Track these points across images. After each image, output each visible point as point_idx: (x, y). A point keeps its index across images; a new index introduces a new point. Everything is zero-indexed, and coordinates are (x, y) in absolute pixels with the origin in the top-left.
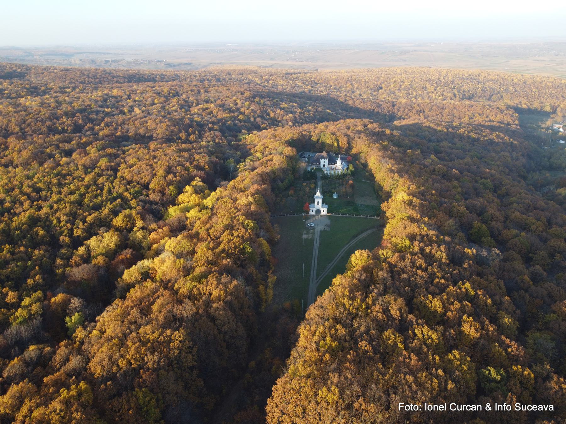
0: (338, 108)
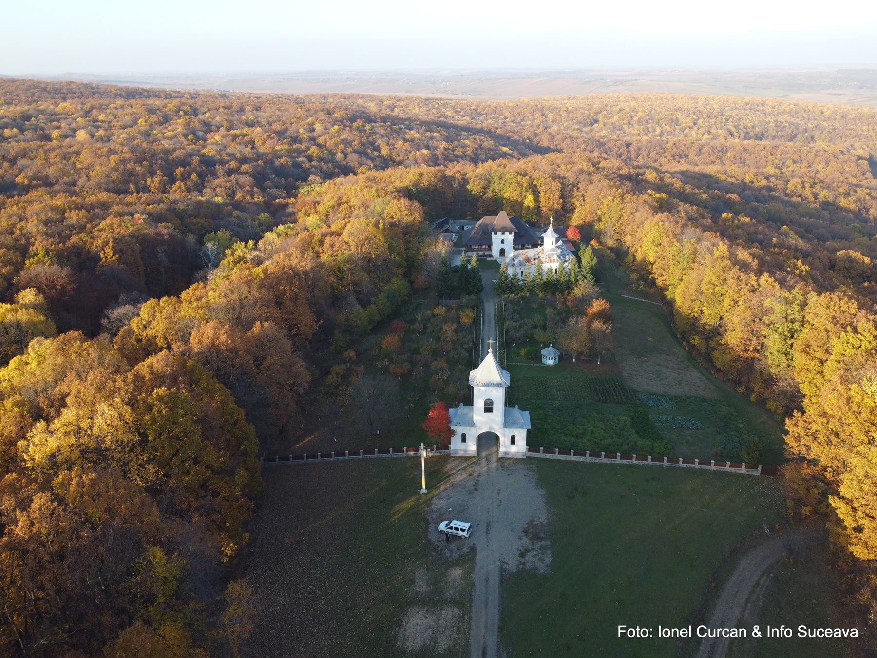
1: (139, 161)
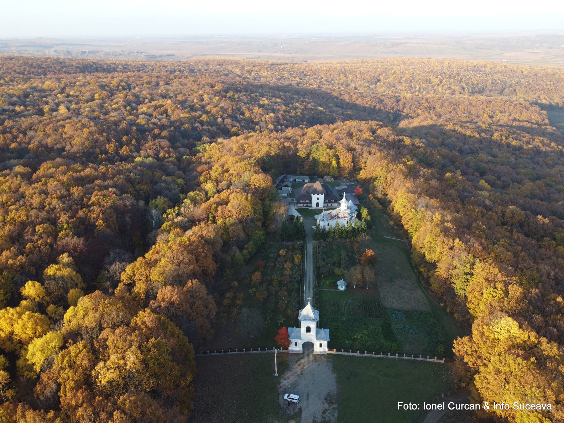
0: (332, 105)
1: (101, 132)
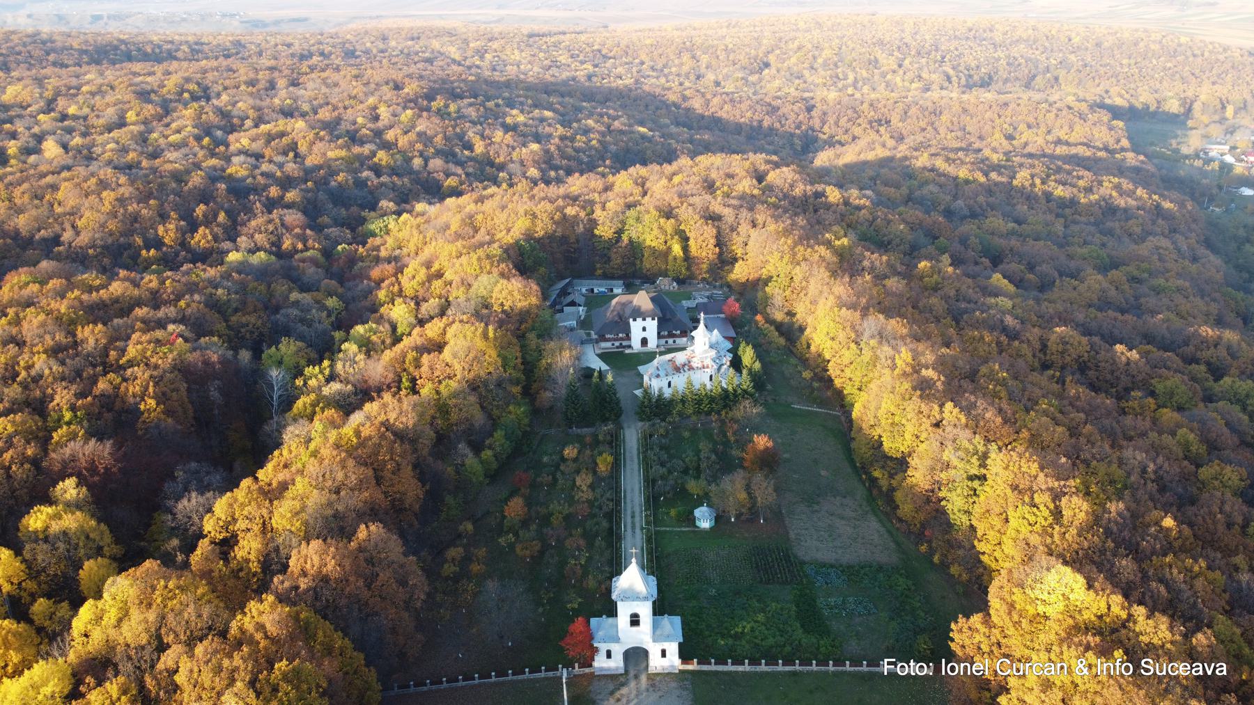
1: (144, 198)
